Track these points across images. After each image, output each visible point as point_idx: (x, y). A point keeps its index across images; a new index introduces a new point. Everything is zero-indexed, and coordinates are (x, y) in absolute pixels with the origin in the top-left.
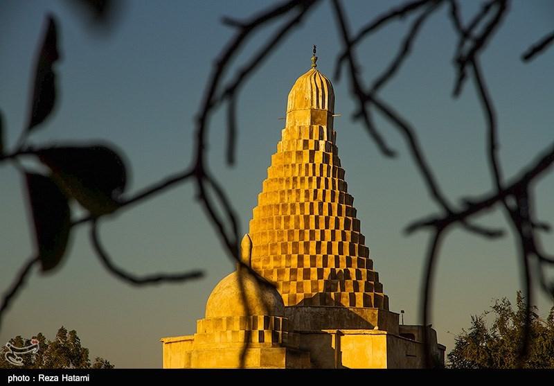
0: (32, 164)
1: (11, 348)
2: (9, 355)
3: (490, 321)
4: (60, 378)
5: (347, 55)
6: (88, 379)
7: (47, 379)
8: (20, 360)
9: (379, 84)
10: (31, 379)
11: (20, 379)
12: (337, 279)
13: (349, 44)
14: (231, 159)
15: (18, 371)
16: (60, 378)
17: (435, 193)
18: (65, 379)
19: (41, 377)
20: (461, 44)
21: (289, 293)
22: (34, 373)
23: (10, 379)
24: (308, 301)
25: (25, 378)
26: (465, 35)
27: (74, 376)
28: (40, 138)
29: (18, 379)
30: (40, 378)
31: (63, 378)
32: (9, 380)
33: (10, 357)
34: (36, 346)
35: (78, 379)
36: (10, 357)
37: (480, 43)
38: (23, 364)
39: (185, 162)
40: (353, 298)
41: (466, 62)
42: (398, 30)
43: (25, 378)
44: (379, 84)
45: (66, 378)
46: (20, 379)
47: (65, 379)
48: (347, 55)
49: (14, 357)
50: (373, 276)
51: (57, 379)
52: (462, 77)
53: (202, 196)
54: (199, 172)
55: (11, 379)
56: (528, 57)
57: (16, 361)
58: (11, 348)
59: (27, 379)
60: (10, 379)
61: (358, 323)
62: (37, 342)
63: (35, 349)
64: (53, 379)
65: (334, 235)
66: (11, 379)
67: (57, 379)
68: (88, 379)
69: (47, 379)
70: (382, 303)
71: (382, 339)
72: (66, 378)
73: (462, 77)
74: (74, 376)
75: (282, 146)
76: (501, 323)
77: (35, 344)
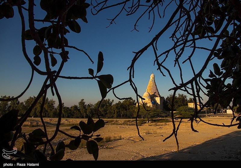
0: (98, 79)
1: (5, 151)
2: (4, 154)
3: (169, 97)
4: (26, 165)
5: (157, 60)
6: (38, 165)
7: (20, 165)
8: (9, 157)
9: (162, 63)
10: (14, 165)
11: (9, 165)
12: (155, 93)
13: (157, 58)
14: (133, 77)
15: (8, 161)
16: (26, 165)
17: (174, 83)
18: (28, 165)
19: (18, 164)
20: (176, 56)
21: (151, 94)
22: (14, 162)
23: (5, 165)
24: (153, 95)
25: (11, 165)
26: (177, 55)
27: (32, 164)
28: (99, 74)
29: (8, 165)
30: (17, 164)
31: (27, 164)
32: (4, 166)
33: (4, 156)
34: (16, 151)
35: (34, 165)
36: (4, 156)
37: (180, 56)
38: (10, 159)
39: (128, 79)
40: (156, 94)
41: (177, 60)
42: (165, 55)
43: (11, 165)
44: (162, 63)
45: (29, 164)
46: (9, 165)
47: (28, 165)
48: (157, 60)
49: (6, 155)
50: (158, 92)
51: (25, 165)
52: (175, 63)
53: (131, 84)
54: (130, 80)
55: (5, 165)
56: (183, 63)
57: (7, 157)
58: (5, 151)
59: (12, 165)
60: (5, 165)
61: (157, 97)
62: (16, 149)
63: (15, 152)
64: (23, 165)
65: (155, 88)
66: (5, 165)
67: (25, 165)
68: (38, 165)
69: (20, 165)
70: (159, 95)
71: (159, 98)
72: (29, 164)
73: (175, 63)
74: (32, 164)
75: (150, 81)
76: (170, 96)
77: (15, 150)
